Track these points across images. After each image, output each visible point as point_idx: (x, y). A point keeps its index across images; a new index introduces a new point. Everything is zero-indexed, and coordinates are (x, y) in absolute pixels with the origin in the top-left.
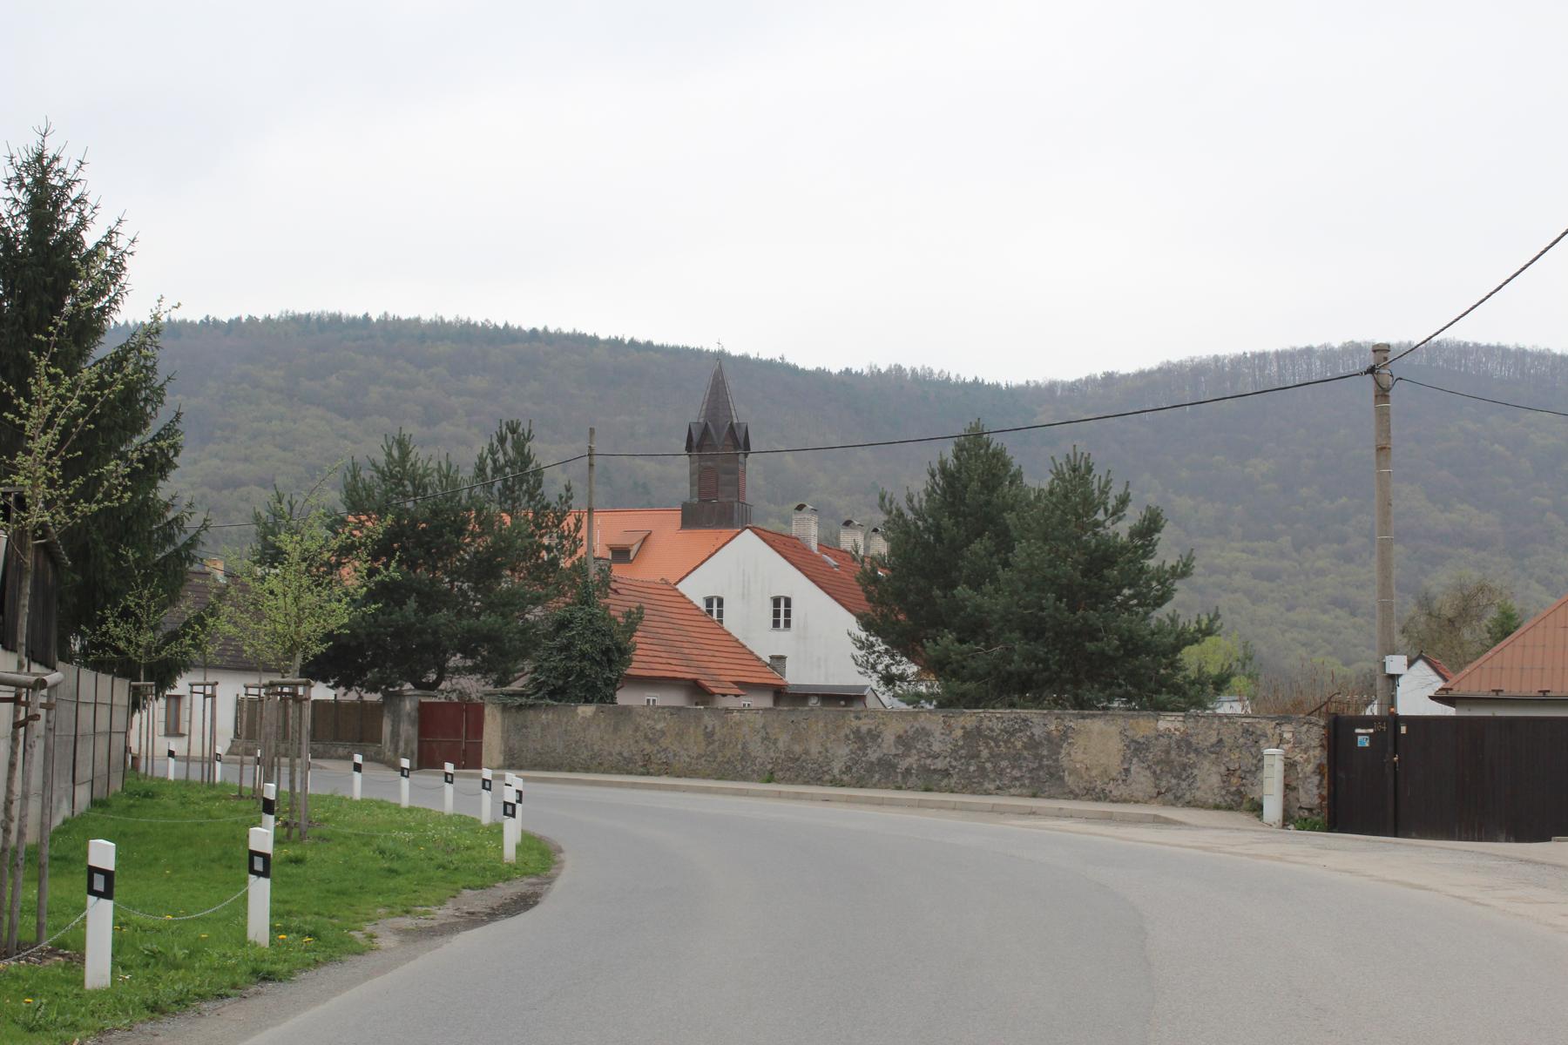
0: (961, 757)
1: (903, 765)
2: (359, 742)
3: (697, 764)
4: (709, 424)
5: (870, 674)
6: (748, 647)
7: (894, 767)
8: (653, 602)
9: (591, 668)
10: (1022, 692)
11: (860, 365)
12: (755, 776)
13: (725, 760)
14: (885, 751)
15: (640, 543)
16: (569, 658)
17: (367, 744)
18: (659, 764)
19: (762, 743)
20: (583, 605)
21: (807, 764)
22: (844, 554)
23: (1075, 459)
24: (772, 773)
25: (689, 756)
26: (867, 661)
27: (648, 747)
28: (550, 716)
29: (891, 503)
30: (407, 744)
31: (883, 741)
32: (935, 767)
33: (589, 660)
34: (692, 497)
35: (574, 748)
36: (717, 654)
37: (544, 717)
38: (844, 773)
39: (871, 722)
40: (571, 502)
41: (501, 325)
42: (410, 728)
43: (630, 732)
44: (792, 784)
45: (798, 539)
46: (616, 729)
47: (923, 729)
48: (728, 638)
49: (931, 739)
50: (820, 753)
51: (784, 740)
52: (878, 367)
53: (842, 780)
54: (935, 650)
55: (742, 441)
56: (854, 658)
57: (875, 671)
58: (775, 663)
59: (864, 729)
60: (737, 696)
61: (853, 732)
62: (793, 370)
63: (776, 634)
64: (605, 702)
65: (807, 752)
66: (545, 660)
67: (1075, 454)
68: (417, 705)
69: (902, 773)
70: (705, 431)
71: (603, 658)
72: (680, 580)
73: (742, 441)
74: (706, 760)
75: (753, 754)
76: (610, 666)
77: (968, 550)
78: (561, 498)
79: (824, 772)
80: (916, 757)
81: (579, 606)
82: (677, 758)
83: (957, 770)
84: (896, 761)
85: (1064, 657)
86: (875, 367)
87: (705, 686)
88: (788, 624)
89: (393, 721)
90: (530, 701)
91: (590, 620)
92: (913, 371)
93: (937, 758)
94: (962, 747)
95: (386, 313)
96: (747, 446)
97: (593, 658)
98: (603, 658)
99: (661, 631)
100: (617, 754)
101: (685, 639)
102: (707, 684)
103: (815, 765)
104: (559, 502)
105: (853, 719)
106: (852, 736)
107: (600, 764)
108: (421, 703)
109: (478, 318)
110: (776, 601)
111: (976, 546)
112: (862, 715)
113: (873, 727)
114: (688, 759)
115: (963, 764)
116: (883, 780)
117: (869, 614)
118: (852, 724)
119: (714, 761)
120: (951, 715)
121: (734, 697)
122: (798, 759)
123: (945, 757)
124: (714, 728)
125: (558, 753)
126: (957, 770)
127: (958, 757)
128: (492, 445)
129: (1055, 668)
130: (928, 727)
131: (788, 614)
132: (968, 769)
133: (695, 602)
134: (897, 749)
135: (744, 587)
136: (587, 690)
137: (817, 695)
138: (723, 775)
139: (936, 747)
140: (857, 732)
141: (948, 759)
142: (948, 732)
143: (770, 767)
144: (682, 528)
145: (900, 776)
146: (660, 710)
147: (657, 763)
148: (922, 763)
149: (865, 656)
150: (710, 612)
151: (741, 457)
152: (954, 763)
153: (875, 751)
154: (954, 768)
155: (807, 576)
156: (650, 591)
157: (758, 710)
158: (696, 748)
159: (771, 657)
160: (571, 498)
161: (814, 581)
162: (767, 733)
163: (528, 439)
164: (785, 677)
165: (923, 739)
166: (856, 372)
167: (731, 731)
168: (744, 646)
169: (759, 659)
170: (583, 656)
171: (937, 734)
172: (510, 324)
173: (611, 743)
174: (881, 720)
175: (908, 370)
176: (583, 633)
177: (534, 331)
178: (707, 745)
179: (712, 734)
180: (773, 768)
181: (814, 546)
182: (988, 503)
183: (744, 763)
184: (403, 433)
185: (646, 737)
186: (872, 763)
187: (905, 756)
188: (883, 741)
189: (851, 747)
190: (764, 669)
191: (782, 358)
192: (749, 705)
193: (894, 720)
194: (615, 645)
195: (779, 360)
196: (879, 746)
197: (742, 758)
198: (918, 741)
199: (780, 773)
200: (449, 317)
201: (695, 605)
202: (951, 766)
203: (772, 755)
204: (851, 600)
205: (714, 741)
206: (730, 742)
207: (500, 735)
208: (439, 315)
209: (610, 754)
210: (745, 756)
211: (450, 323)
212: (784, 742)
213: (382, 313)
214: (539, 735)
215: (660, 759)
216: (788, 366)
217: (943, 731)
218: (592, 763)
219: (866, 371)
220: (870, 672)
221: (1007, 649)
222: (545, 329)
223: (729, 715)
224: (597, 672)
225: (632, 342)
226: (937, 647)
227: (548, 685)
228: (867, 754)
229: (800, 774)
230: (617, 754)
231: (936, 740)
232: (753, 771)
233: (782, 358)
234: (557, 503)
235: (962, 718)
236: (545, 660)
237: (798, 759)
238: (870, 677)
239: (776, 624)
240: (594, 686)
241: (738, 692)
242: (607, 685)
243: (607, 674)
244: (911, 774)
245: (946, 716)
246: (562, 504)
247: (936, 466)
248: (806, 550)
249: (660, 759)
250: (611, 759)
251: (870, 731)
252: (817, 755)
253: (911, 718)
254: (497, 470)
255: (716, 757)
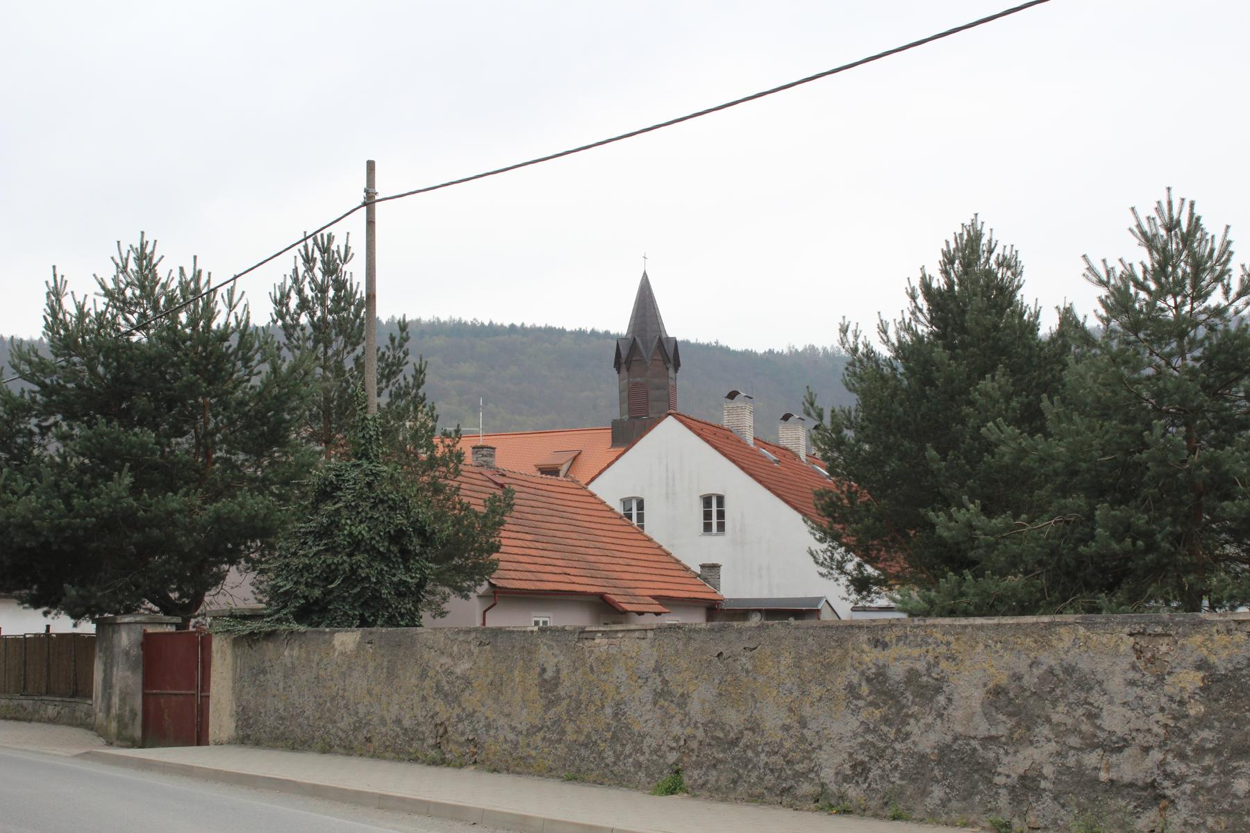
0: (1200, 751)
1: (1014, 764)
2: (72, 696)
3: (528, 745)
4: (638, 340)
5: (836, 576)
6: (673, 555)
7: (987, 770)
8: (551, 500)
9: (370, 566)
10: (1111, 588)
11: (781, 347)
12: (641, 774)
13: (582, 738)
14: (959, 729)
15: (570, 462)
16: (332, 549)
17: (79, 700)
18: (461, 745)
19: (655, 704)
20: (360, 459)
21: (757, 754)
22: (784, 451)
23: (1170, 209)
24: (677, 772)
25: (513, 729)
26: (832, 558)
27: (440, 706)
28: (295, 653)
29: (856, 337)
30: (123, 700)
31: (950, 700)
32: (1113, 775)
33: (367, 551)
34: (622, 414)
35: (329, 710)
36: (634, 562)
37: (290, 654)
38: (846, 779)
39: (916, 652)
40: (407, 345)
41: (486, 323)
42: (129, 673)
43: (414, 681)
44: (724, 800)
45: (731, 431)
46: (391, 674)
47: (1069, 670)
48: (648, 544)
49: (1096, 697)
50: (786, 728)
51: (701, 696)
52: (796, 347)
53: (842, 797)
54: (949, 529)
55: (671, 355)
56: (812, 554)
57: (843, 572)
58: (706, 573)
59: (897, 671)
60: (657, 614)
61: (869, 680)
62: (726, 351)
63: (708, 539)
64: (398, 625)
65: (755, 727)
66: (295, 554)
67: (1170, 203)
68: (140, 638)
69: (1012, 789)
70: (633, 346)
71: (392, 548)
72: (593, 480)
73: (671, 355)
74: (544, 739)
75: (636, 729)
76: (406, 561)
77: (976, 390)
78: (392, 339)
79: (798, 775)
80: (1052, 747)
81: (354, 460)
82: (492, 732)
83: (1188, 788)
84: (991, 755)
85: (1179, 529)
86: (793, 347)
87: (614, 602)
88: (721, 527)
89: (105, 664)
90: (267, 628)
91: (369, 485)
92: (825, 349)
93: (1120, 750)
94: (1202, 722)
95: (393, 317)
96: (677, 365)
97: (373, 547)
98: (392, 548)
99: (559, 534)
100: (394, 722)
101: (591, 544)
102: (617, 599)
103: (774, 758)
104: (390, 346)
105: (865, 647)
106: (865, 689)
107: (368, 740)
108: (147, 636)
109: (468, 318)
110: (707, 500)
111: (986, 384)
112: (889, 636)
113: (921, 666)
114: (511, 736)
115: (1207, 771)
116: (955, 804)
117: (831, 492)
118: (866, 659)
119: (559, 741)
120: (1159, 630)
121: (655, 616)
122: (734, 743)
123: (1146, 750)
124: (558, 671)
125: (308, 718)
126: (1188, 788)
127: (1189, 751)
128: (296, 270)
129: (1165, 545)
130: (1084, 665)
131: (721, 515)
132: (1226, 785)
133: (608, 503)
134: (993, 722)
135: (667, 485)
136: (365, 605)
137: (759, 611)
138: (579, 771)
139: (1114, 721)
140: (878, 678)
141: (1156, 755)
142: (1150, 679)
143: (672, 757)
144: (612, 446)
145: (1004, 799)
146: (461, 637)
147: (457, 742)
148: (1071, 761)
149: (827, 550)
150: (630, 517)
151: (671, 372)
152: (1177, 767)
153: (929, 727)
154: (1178, 781)
155: (743, 468)
156: (549, 488)
157: (646, 630)
158: (524, 712)
159: (703, 566)
160: (407, 339)
161: (751, 475)
162: (665, 682)
163: (345, 261)
164: (719, 590)
165: (1072, 698)
166: (778, 352)
167: (591, 677)
168: (668, 554)
169: (687, 569)
170: (356, 544)
171: (1116, 684)
172: (494, 323)
173: (384, 698)
174: (943, 649)
175: (820, 349)
176: (357, 506)
177: (513, 326)
178: (547, 708)
179: (556, 682)
180: (679, 760)
181: (750, 441)
182: (996, 327)
183: (619, 748)
184: (197, 270)
185: (439, 689)
186: (923, 757)
187: (1014, 742)
188: (950, 700)
189: (863, 715)
190: (693, 581)
191: (717, 343)
192: (545, 623)
193: (980, 647)
194: (412, 524)
195: (714, 344)
196: (941, 716)
197: (614, 736)
198: (1054, 703)
199: (696, 773)
200: (444, 318)
201: (608, 506)
202: (1167, 775)
203: (677, 730)
204: (795, 497)
205: (559, 699)
206: (591, 701)
207: (231, 684)
208: (436, 316)
209: (383, 722)
210: (620, 733)
211: (445, 323)
212: (703, 702)
213: (390, 317)
214: (281, 685)
215: (463, 734)
216: (721, 347)
217: (1132, 675)
218: (356, 738)
219: (786, 351)
220: (836, 573)
221: (1068, 522)
222: (523, 324)
223: (588, 643)
224: (380, 572)
225: (594, 333)
226: (952, 524)
227: (297, 597)
228: (908, 735)
229: (740, 776)
230: (394, 722)
231: (1111, 702)
232: (638, 765)
233: (717, 343)
234: (387, 347)
235: (1198, 638)
236: (295, 554)
237: (734, 743)
238: (837, 580)
239: (707, 527)
240: (376, 597)
241: (659, 608)
242: (400, 595)
243: (401, 575)
244: (1039, 793)
245: (1142, 634)
246: (394, 349)
247: (916, 283)
248: (740, 442)
249: (463, 734)
250: (384, 730)
251: (912, 675)
252: (780, 734)
253: (1029, 641)
254: (304, 305)
255: (563, 732)
